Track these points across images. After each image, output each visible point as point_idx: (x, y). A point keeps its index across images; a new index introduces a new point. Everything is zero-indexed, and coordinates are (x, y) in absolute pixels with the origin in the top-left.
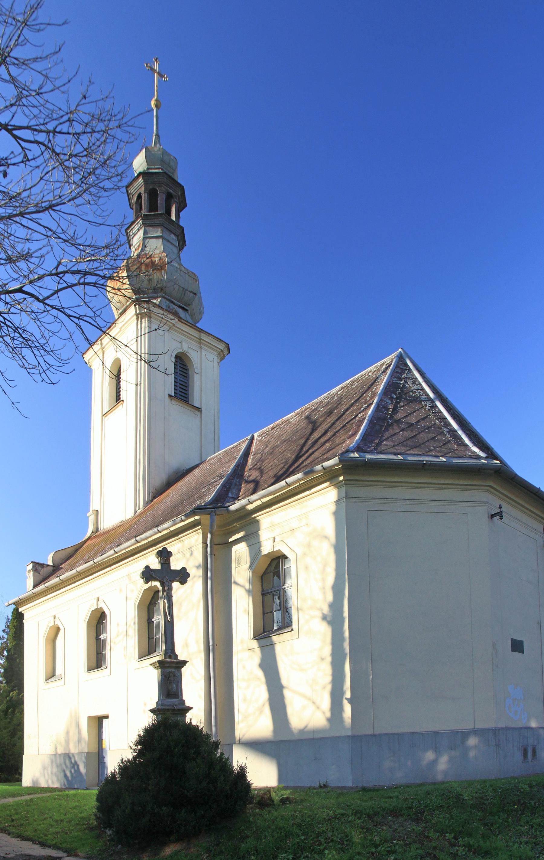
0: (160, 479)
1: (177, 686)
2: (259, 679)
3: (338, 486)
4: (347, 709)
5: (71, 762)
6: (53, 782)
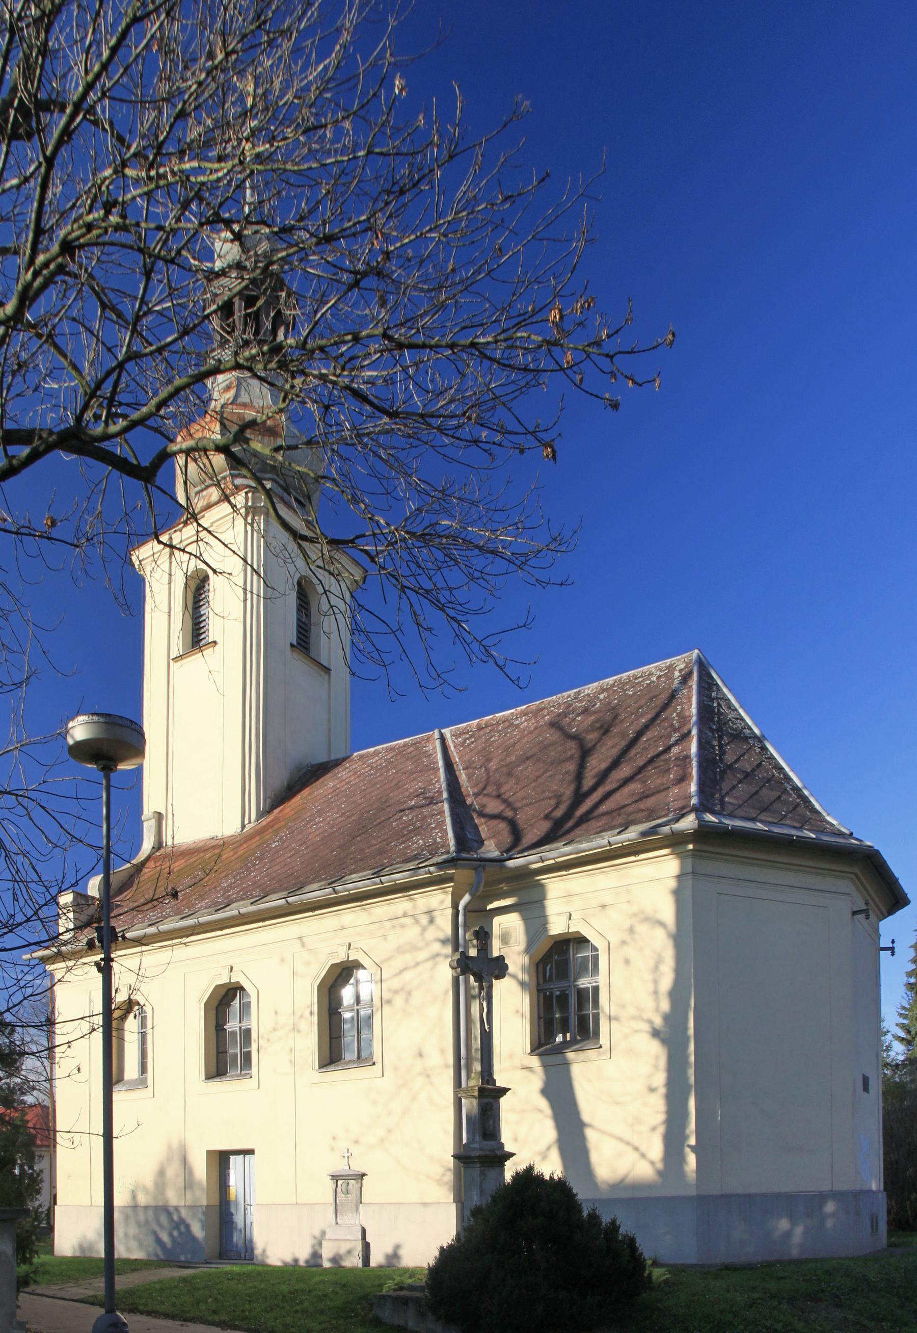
0: (281, 779)
1: (494, 1122)
2: (540, 1111)
3: (681, 856)
4: (692, 1159)
5: (172, 1220)
6: (128, 1249)
